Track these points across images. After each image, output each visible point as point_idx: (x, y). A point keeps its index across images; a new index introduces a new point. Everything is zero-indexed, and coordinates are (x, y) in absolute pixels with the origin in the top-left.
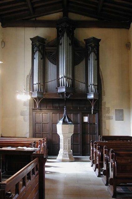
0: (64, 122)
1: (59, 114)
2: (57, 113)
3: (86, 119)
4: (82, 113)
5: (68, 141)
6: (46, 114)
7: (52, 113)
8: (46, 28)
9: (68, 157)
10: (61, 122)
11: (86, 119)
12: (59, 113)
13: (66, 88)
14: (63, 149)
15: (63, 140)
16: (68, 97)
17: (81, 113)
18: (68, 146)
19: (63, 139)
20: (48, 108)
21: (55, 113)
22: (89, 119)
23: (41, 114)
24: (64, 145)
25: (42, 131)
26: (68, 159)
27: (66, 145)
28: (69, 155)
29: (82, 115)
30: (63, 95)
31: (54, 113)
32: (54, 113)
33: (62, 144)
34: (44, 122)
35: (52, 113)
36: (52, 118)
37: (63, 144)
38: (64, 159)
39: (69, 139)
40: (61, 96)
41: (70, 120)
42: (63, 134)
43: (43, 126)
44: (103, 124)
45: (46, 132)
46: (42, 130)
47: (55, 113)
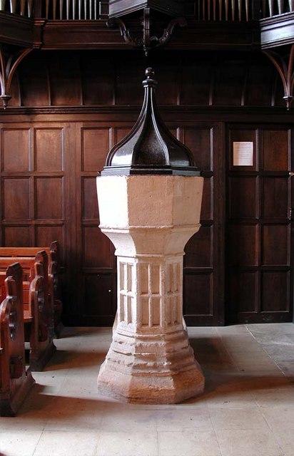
0: (145, 163)
1: (116, 129)
2: (104, 125)
3: (245, 154)
4: (226, 123)
5: (170, 274)
6: (51, 134)
7: (80, 125)
8: (53, 394)
9: (165, 375)
10: (124, 159)
11: (245, 154)
12: (118, 124)
13: (109, 163)
14: (134, 324)
15: (134, 270)
16: (164, 39)
17: (221, 125)
18: (169, 305)
19: (134, 262)
20: (60, 102)
21: (97, 125)
22: (259, 154)
23: (28, 135)
24: (142, 303)
25: (36, 211)
26: (168, 384)
27: (156, 303)
28: (173, 358)
29: (226, 136)
30: (136, 32)
31: (92, 125)
32: (92, 125)
33: (127, 292)
34: (43, 170)
35: (80, 125)
36: (79, 150)
37: (134, 293)
38: (147, 384)
39: (170, 261)
40: (124, 33)
41: (177, 150)
42: (140, 235)
43: (40, 192)
44: (65, 429)
45: (53, 217)
46: (32, 206)
47: (97, 125)
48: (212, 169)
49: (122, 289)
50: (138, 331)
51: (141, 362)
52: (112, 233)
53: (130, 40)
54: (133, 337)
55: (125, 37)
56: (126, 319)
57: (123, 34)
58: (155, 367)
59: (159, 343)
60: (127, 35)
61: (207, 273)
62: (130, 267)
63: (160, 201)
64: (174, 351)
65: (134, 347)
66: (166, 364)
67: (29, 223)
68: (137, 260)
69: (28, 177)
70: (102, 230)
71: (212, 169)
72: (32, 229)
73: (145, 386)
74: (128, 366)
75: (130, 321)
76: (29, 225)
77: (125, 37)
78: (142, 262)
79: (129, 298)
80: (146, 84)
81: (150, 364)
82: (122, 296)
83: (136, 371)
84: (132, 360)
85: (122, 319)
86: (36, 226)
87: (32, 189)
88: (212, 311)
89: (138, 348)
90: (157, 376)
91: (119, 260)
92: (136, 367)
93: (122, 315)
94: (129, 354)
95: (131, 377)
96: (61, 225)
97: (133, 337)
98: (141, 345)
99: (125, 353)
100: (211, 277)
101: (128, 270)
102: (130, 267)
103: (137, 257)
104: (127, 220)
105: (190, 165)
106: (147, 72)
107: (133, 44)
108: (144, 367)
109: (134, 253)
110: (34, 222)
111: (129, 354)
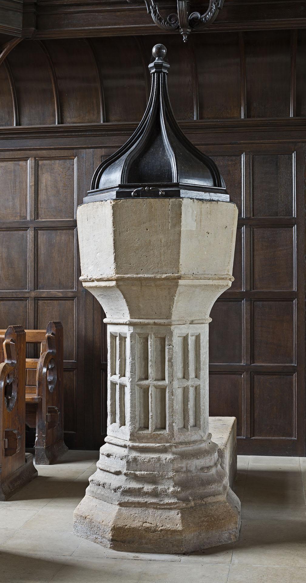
9: (169, 507)
48: (294, 214)
49: (114, 373)
50: (133, 437)
51: (134, 485)
52: (96, 287)
53: (160, 20)
54: (125, 446)
55: (152, 15)
56: (118, 420)
57: (150, 12)
58: (155, 494)
59: (163, 456)
60: (155, 12)
61: (289, 372)
62: (123, 339)
63: (161, 236)
64: (188, 471)
65: (124, 461)
66: (172, 489)
67: (27, 295)
68: (132, 329)
69: (26, 229)
70: (84, 284)
71: (294, 214)
72: (30, 304)
73: (136, 524)
74: (115, 490)
75: (123, 423)
76: (26, 299)
77: (152, 15)
78: (139, 330)
79: (122, 387)
80: (152, 68)
81: (148, 488)
82: (114, 384)
83: (127, 499)
84: (120, 481)
85: (114, 421)
86: (37, 299)
87: (30, 245)
88: (295, 432)
89: (131, 463)
90: (156, 506)
91: (110, 329)
92: (128, 492)
93: (114, 413)
94: (118, 473)
95: (118, 507)
96: (72, 298)
97: (125, 446)
98: (135, 459)
99: (113, 471)
100: (295, 377)
101: (120, 344)
102: (123, 339)
103: (130, 324)
104: (113, 266)
105: (215, 185)
106: (154, 50)
107: (163, 25)
108: (138, 492)
109: (127, 318)
110: (33, 294)
111: (118, 473)
